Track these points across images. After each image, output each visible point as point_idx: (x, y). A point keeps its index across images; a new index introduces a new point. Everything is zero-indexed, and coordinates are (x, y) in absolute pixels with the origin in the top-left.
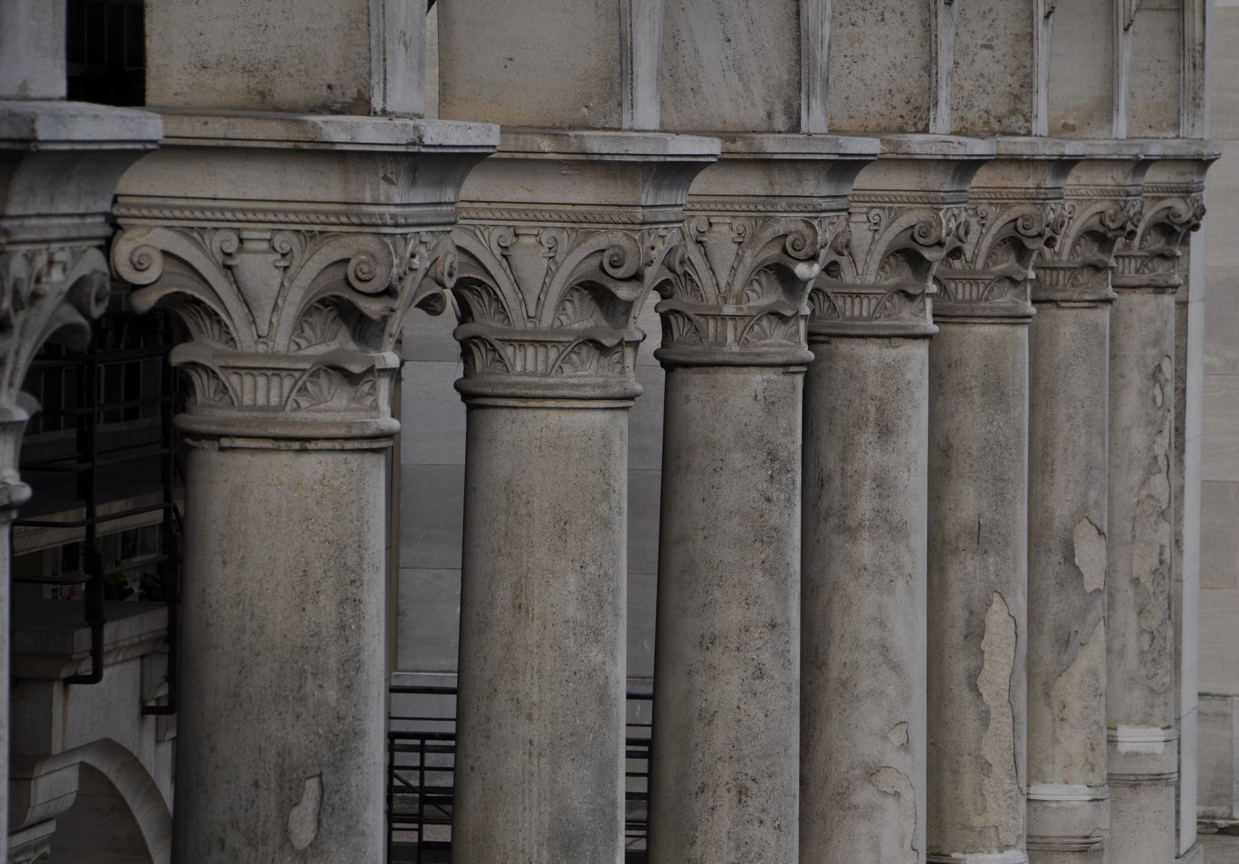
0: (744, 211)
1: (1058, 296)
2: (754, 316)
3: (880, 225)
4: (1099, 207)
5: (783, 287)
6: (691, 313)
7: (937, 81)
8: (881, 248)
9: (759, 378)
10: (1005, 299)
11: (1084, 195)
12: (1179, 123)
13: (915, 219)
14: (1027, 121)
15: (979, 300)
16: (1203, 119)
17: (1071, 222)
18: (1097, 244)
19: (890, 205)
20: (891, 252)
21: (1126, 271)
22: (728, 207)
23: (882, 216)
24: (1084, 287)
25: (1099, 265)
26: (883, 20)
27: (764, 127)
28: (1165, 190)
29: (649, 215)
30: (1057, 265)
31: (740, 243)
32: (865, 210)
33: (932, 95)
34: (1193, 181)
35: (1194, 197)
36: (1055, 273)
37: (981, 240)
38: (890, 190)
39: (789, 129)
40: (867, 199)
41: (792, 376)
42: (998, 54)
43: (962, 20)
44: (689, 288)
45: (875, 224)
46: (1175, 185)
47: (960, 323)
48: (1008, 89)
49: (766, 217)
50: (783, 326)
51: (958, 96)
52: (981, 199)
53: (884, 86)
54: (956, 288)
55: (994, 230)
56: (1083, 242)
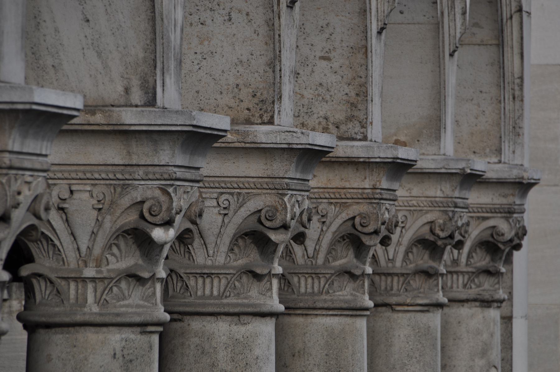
0: (103, 179)
1: (393, 300)
2: (112, 279)
3: (229, 209)
4: (429, 217)
5: (140, 251)
6: (53, 276)
7: (281, 77)
8: (230, 231)
9: (118, 337)
10: (345, 293)
11: (415, 206)
12: (501, 149)
13: (262, 203)
14: (363, 127)
15: (321, 293)
16: (523, 146)
17: (403, 230)
18: (428, 252)
19: (238, 191)
20: (239, 235)
21: (455, 286)
22: (89, 175)
23: (231, 201)
24: (416, 292)
25: (431, 271)
26: (230, 20)
27: (122, 101)
28: (489, 210)
29: (16, 161)
30: (391, 272)
31: (100, 209)
32: (215, 195)
33: (276, 89)
34: (514, 202)
35: (516, 218)
36: (389, 279)
37: (321, 237)
38: (238, 177)
39: (145, 104)
40: (217, 185)
41: (149, 335)
42: (336, 65)
43: (301, 33)
44: (51, 253)
45: (225, 208)
46: (499, 206)
47: (303, 315)
48: (345, 98)
49: (124, 185)
50: (141, 288)
51: (299, 104)
52: (321, 198)
53: (232, 81)
54: (299, 282)
55: (334, 228)
56: (415, 250)
